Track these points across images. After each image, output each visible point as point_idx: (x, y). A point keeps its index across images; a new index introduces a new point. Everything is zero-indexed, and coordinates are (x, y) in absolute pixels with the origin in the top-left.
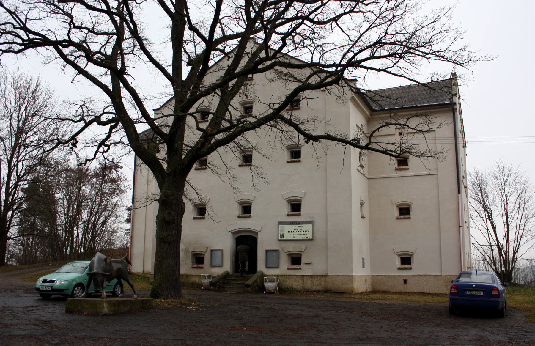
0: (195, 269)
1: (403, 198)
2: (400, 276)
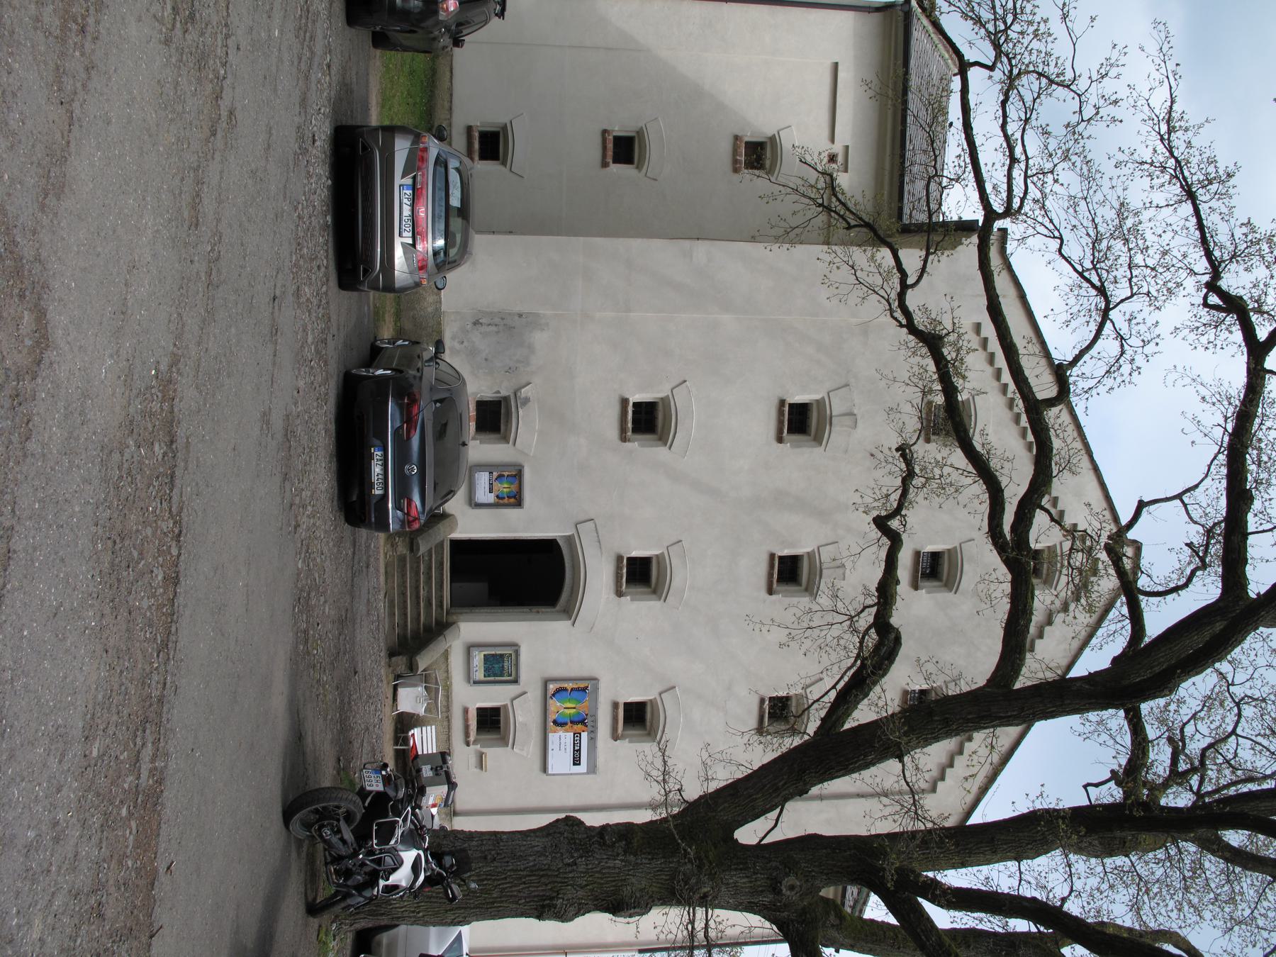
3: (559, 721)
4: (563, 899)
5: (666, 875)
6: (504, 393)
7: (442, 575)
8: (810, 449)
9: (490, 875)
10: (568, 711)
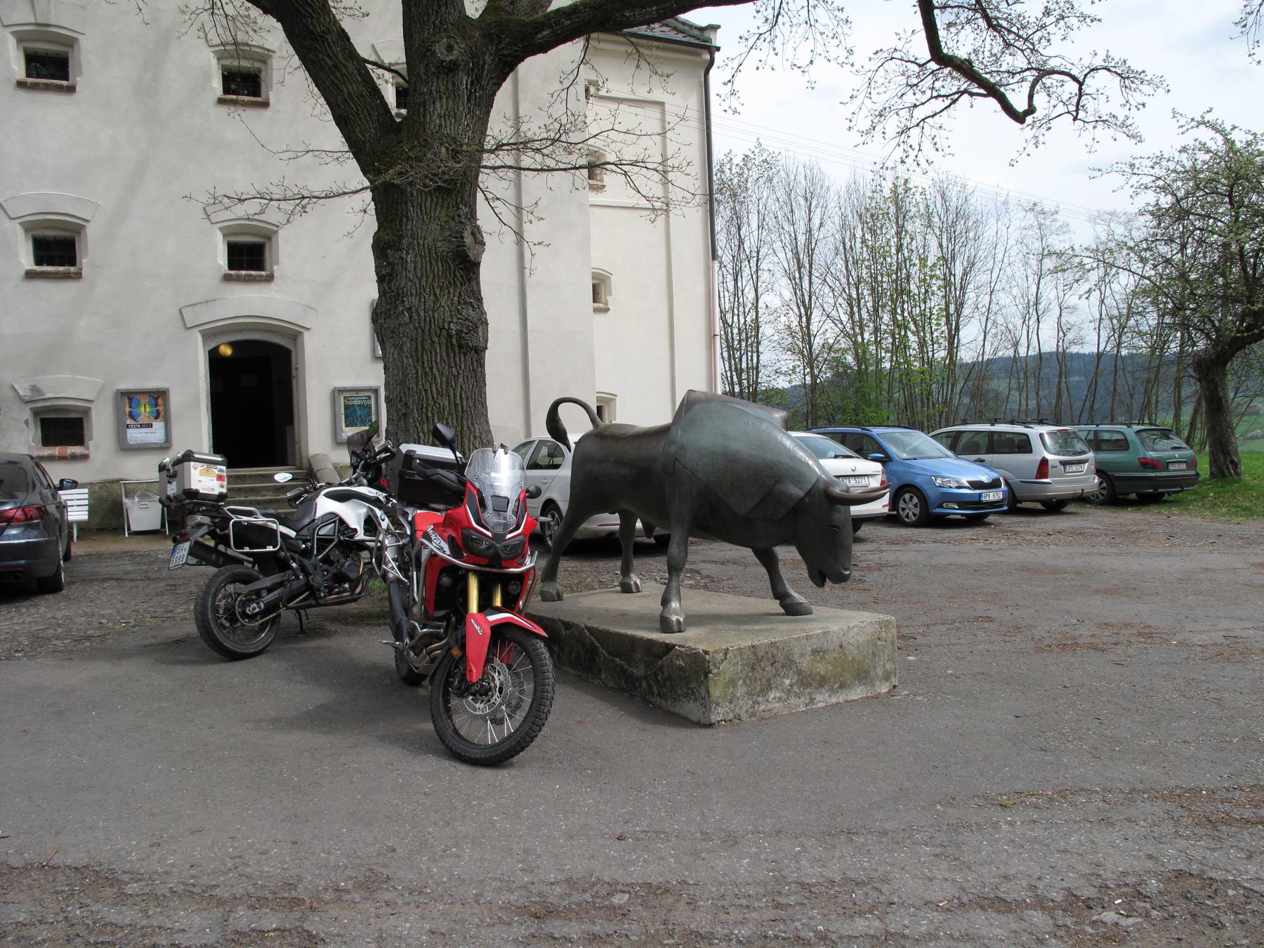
4: (450, 322)
5: (426, 199)
6: (27, 414)
7: (251, 476)
8: (83, 52)
9: (421, 409)
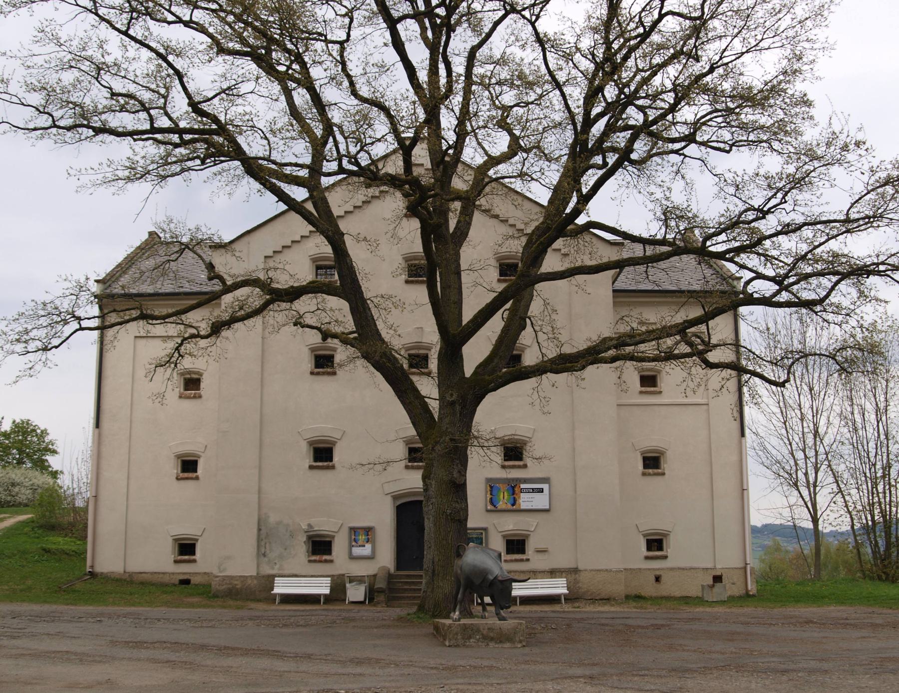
0: (313, 565)
1: (651, 442)
2: (649, 569)
3: (513, 502)
7: (414, 575)
10: (506, 497)
